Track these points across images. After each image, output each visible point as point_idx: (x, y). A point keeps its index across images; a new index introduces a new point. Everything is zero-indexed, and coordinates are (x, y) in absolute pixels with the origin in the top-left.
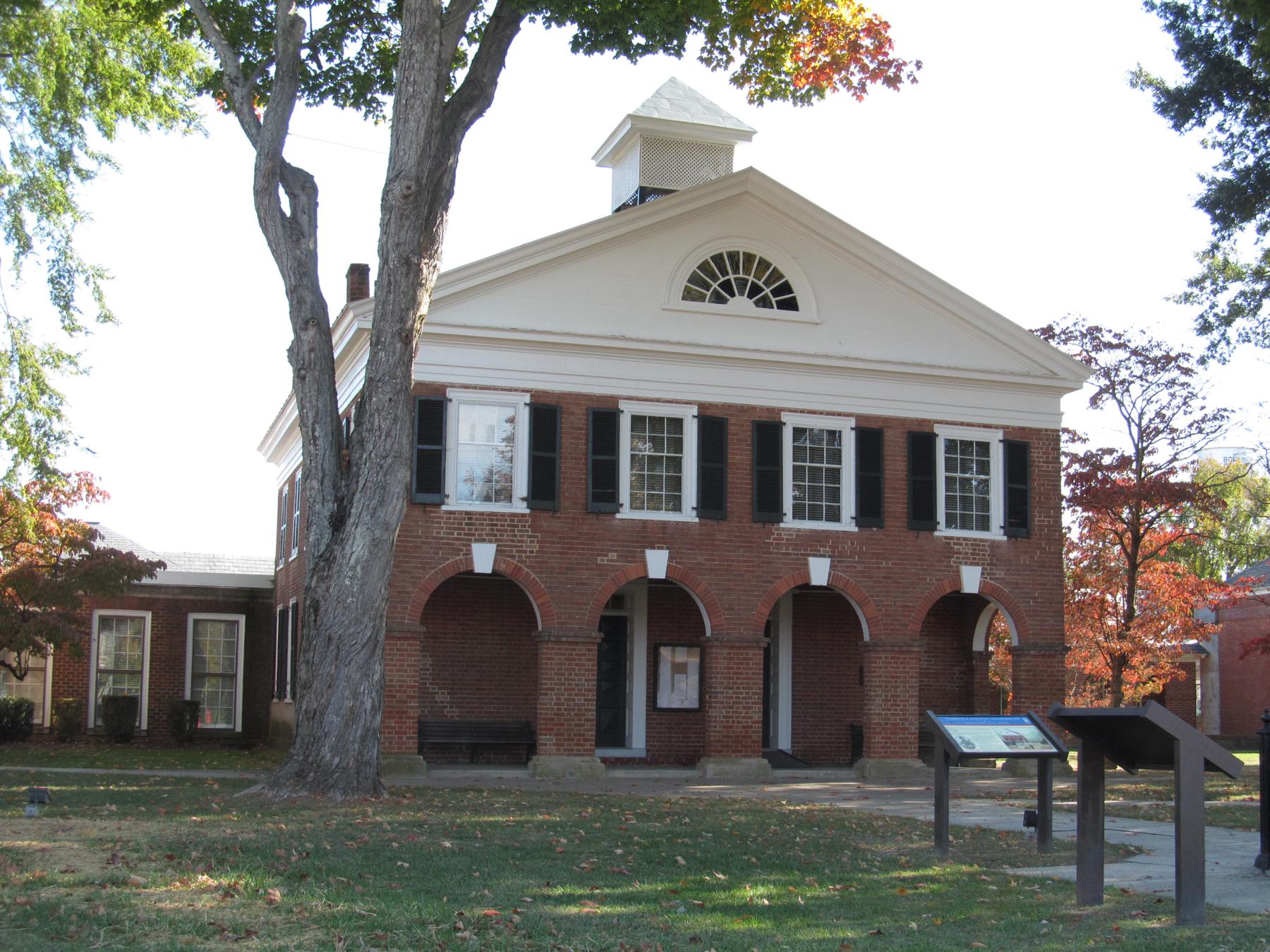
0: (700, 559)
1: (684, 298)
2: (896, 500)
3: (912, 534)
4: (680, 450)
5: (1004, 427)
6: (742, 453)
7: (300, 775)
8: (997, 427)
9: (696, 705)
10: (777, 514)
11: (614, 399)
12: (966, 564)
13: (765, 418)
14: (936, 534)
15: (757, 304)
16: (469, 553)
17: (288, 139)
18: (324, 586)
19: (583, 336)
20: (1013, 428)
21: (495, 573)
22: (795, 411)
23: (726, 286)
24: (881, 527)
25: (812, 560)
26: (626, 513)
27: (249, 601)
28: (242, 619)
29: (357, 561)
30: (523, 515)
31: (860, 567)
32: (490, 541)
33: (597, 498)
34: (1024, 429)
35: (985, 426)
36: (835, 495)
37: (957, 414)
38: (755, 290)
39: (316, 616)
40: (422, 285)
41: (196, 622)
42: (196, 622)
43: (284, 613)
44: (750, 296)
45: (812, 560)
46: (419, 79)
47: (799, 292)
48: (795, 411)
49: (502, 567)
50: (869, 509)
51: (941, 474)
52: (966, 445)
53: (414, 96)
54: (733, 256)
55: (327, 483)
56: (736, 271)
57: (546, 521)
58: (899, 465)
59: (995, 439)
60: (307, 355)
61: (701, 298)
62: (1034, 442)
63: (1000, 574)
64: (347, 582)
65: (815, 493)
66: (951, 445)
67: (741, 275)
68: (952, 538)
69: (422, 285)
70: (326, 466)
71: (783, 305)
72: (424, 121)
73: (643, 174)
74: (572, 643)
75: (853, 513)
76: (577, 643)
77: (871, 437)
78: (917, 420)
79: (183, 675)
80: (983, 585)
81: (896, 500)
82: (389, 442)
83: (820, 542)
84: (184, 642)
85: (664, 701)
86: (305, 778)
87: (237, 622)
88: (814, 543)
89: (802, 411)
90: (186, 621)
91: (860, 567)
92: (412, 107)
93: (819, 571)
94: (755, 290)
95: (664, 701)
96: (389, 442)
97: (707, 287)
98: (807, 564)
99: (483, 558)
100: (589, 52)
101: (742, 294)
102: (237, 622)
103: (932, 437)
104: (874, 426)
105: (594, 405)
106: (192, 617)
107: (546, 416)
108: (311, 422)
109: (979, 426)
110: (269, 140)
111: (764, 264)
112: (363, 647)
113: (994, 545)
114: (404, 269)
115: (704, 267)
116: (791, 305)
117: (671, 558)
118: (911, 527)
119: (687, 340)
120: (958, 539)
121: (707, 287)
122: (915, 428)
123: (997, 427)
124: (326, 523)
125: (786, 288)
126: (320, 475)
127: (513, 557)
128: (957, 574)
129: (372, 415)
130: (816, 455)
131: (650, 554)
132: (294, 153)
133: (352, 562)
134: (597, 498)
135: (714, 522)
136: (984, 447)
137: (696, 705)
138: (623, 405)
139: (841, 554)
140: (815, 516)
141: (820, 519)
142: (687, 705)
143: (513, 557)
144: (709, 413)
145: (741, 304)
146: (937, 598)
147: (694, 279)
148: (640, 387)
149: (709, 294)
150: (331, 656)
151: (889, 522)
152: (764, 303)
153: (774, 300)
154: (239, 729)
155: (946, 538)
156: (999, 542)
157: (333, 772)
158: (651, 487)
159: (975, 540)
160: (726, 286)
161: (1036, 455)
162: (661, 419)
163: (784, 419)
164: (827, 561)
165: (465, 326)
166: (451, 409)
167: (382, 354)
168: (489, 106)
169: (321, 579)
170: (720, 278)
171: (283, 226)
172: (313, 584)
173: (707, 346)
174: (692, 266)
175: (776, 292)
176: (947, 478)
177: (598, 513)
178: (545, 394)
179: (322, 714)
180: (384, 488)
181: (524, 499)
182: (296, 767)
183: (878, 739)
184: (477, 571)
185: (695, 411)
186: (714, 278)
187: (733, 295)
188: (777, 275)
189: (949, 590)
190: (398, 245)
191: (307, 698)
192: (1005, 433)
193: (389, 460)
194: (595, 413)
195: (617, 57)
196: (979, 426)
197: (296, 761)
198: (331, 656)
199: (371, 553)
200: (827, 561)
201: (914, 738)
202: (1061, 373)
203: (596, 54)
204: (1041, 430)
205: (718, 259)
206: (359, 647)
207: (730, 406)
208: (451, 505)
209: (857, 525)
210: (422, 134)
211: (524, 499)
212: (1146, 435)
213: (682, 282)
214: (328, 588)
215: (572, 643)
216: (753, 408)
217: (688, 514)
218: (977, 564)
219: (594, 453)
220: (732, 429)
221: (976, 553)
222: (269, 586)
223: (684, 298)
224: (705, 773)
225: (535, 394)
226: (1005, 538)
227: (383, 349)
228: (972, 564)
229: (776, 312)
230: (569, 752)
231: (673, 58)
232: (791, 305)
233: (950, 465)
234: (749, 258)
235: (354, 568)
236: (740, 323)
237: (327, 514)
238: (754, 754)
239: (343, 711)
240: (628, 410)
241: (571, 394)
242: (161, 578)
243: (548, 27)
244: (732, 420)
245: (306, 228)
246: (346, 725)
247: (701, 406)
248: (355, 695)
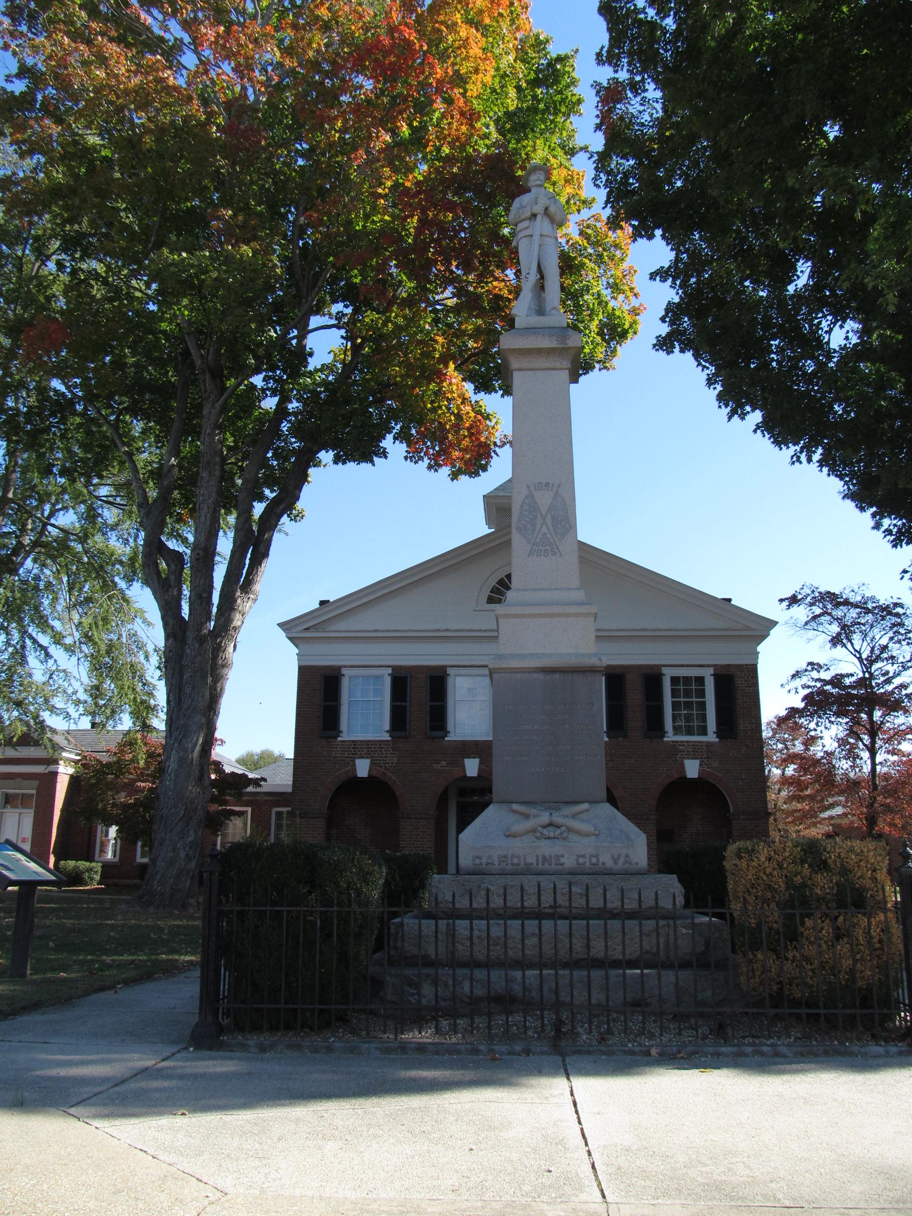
1: (488, 603)
2: (635, 717)
4: (703, 696)
5: (714, 666)
8: (709, 666)
10: (661, 732)
11: (659, 667)
12: (688, 758)
14: (665, 739)
16: (354, 765)
19: (366, 631)
20: (721, 666)
21: (370, 776)
24: (625, 737)
30: (387, 741)
32: (367, 758)
33: (432, 728)
36: (704, 718)
37: (675, 659)
40: (235, 609)
41: (277, 813)
42: (277, 813)
49: (374, 773)
52: (687, 680)
65: (688, 718)
66: (675, 680)
68: (677, 742)
69: (235, 609)
72: (209, 515)
74: (418, 818)
76: (421, 818)
78: (649, 665)
81: (635, 717)
99: (692, 769)
107: (401, 681)
109: (695, 666)
112: (180, 820)
113: (709, 745)
117: (481, 763)
119: (468, 628)
120: (682, 742)
123: (709, 666)
127: (381, 767)
134: (432, 728)
136: (700, 680)
138: (664, 670)
140: (689, 732)
141: (694, 735)
143: (381, 767)
155: (673, 742)
156: (714, 742)
159: (694, 742)
165: (347, 631)
166: (450, 681)
168: (298, 499)
171: (159, 583)
173: (383, 631)
176: (673, 702)
177: (434, 738)
181: (387, 732)
184: (689, 776)
189: (676, 777)
192: (715, 670)
193: (190, 711)
194: (431, 677)
196: (695, 666)
199: (179, 766)
204: (742, 665)
208: (344, 737)
209: (717, 737)
210: (208, 523)
211: (387, 732)
212: (868, 663)
213: (486, 592)
215: (418, 818)
218: (696, 758)
219: (431, 701)
220: (738, 682)
221: (695, 751)
223: (488, 603)
225: (395, 669)
226: (717, 740)
228: (692, 758)
233: (674, 693)
240: (668, 673)
242: (265, 787)
248: (174, 849)
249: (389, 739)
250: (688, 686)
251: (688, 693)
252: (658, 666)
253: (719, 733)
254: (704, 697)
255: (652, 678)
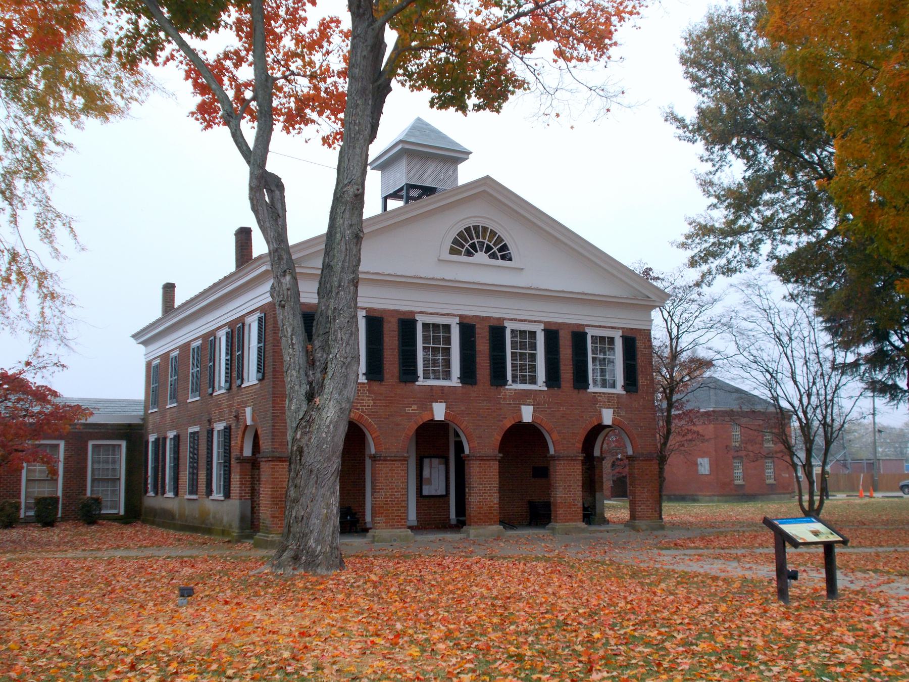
0: (463, 408)
3: (576, 391)
6: (485, 348)
7: (296, 558)
9: (444, 493)
13: (495, 324)
15: (490, 256)
17: (269, 155)
18: (306, 438)
22: (512, 320)
23: (473, 246)
24: (559, 387)
25: (523, 407)
26: (421, 382)
27: (132, 434)
28: (124, 444)
29: (331, 422)
30: (364, 384)
31: (548, 411)
34: (632, 329)
35: (612, 328)
36: (533, 368)
37: (598, 322)
38: (489, 249)
39: (301, 456)
43: (160, 443)
44: (486, 253)
45: (523, 407)
46: (362, 121)
47: (512, 249)
48: (512, 320)
50: (553, 377)
51: (590, 356)
52: (436, 326)
53: (359, 132)
54: (476, 228)
55: (302, 372)
56: (478, 237)
57: (376, 386)
58: (569, 352)
59: (454, 323)
60: (285, 292)
61: (459, 253)
62: (638, 337)
63: (623, 413)
64: (324, 435)
66: (426, 326)
67: (481, 240)
70: (301, 361)
71: (503, 258)
73: (408, 177)
75: (544, 380)
77: (468, 329)
79: (85, 480)
80: (614, 420)
82: (348, 349)
83: (526, 398)
84: (86, 459)
85: (426, 492)
86: (300, 559)
87: (120, 445)
88: (524, 397)
89: (516, 320)
90: (87, 445)
91: (548, 411)
92: (358, 139)
93: (527, 414)
94: (489, 249)
95: (426, 492)
96: (348, 349)
97: (463, 246)
98: (520, 410)
100: (440, 108)
101: (481, 251)
102: (120, 445)
103: (414, 322)
104: (554, 328)
105: (402, 317)
106: (91, 444)
108: (289, 334)
109: (609, 327)
110: (256, 157)
111: (493, 233)
114: (355, 241)
115: (460, 234)
116: (506, 257)
118: (575, 387)
121: (463, 246)
122: (576, 330)
124: (303, 398)
125: (504, 248)
126: (297, 367)
128: (600, 413)
129: (336, 331)
130: (523, 346)
131: (435, 405)
132: (271, 166)
133: (327, 423)
135: (470, 386)
136: (533, 334)
137: (444, 493)
138: (506, 324)
139: (538, 404)
140: (523, 382)
142: (439, 493)
144: (465, 321)
145: (481, 257)
146: (590, 428)
147: (455, 241)
148: (429, 308)
149: (464, 250)
150: (312, 482)
151: (563, 384)
152: (493, 256)
153: (499, 254)
154: (122, 512)
157: (318, 555)
158: (434, 366)
160: (473, 246)
161: (639, 344)
162: (525, 332)
163: (417, 318)
164: (531, 408)
167: (342, 293)
169: (304, 434)
170: (470, 241)
172: (298, 437)
174: (453, 234)
175: (500, 250)
178: (374, 310)
179: (308, 519)
180: (346, 376)
182: (292, 553)
183: (561, 511)
185: (457, 320)
186: (467, 241)
187: (476, 251)
188: (500, 239)
190: (351, 225)
191: (296, 509)
193: (349, 359)
195: (457, 110)
197: (291, 549)
198: (312, 482)
200: (531, 408)
201: (580, 510)
202: (653, 298)
203: (443, 110)
205: (468, 230)
206: (329, 475)
207: (477, 317)
209: (461, 382)
213: (448, 244)
214: (310, 439)
216: (489, 318)
217: (455, 381)
220: (478, 331)
221: (611, 401)
222: (141, 422)
224: (468, 535)
227: (343, 290)
229: (500, 262)
230: (393, 527)
231: (495, 113)
232: (506, 257)
233: (426, 339)
234: (485, 229)
235: (328, 427)
236: (480, 269)
237: (304, 392)
238: (495, 523)
239: (321, 517)
240: (421, 320)
241: (388, 310)
243: (412, 91)
244: (478, 326)
245: (280, 212)
246: (324, 525)
247: (461, 317)
249: (366, 381)
250: (438, 332)
251: (436, 340)
252: (582, 325)
253: (625, 387)
254: (535, 350)
255: (407, 325)
